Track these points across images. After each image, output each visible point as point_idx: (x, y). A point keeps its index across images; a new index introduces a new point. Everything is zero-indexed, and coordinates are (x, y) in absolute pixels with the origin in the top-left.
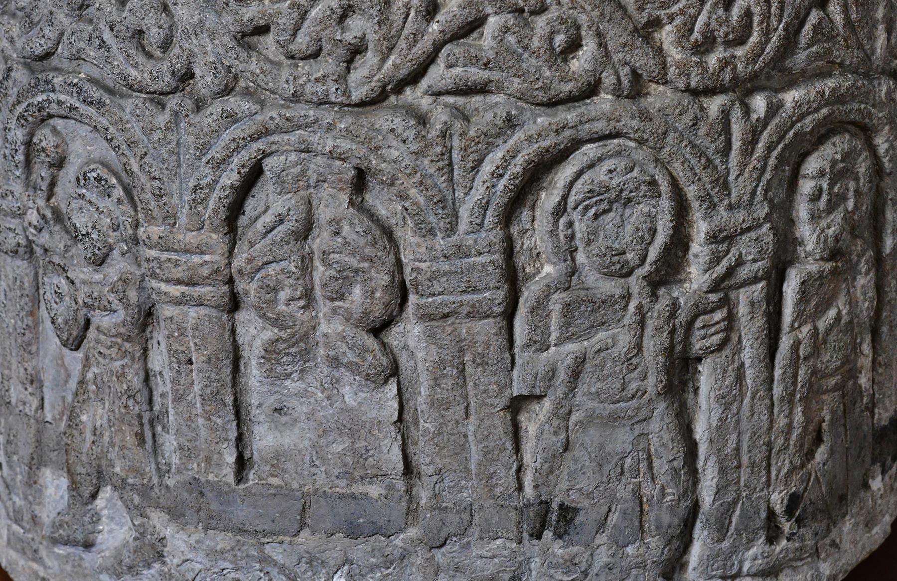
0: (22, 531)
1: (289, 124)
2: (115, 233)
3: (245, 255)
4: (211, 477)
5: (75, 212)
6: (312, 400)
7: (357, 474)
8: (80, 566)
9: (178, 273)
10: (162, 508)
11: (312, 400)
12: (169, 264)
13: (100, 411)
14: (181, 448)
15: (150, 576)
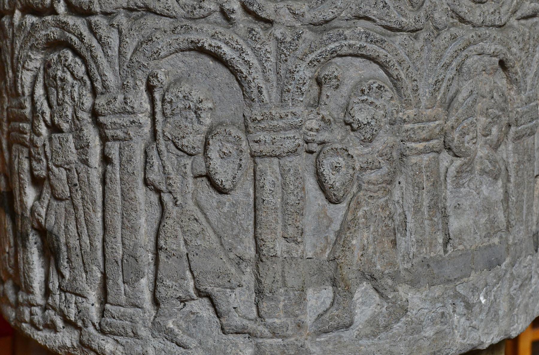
0: (280, 340)
1: (479, 39)
2: (385, 119)
3: (453, 118)
4: (432, 255)
5: (356, 112)
6: (472, 197)
7: (492, 233)
8: (340, 342)
9: (424, 134)
10: (406, 282)
11: (472, 197)
12: (419, 131)
13: (366, 234)
14: (418, 242)
15: (398, 328)
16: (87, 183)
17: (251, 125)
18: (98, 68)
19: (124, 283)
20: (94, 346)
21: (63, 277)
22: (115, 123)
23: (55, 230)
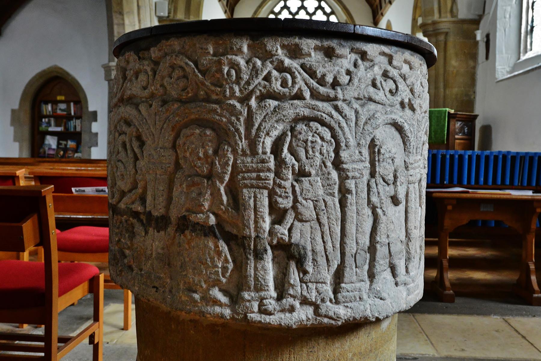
16: (333, 208)
17: (410, 166)
18: (344, 134)
19: (356, 267)
20: (331, 314)
21: (305, 272)
22: (355, 169)
23: (302, 242)
